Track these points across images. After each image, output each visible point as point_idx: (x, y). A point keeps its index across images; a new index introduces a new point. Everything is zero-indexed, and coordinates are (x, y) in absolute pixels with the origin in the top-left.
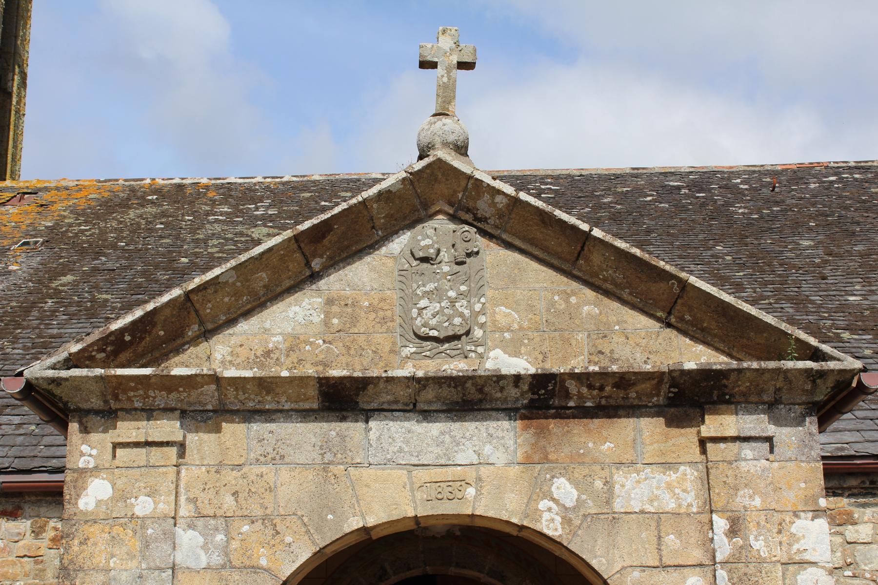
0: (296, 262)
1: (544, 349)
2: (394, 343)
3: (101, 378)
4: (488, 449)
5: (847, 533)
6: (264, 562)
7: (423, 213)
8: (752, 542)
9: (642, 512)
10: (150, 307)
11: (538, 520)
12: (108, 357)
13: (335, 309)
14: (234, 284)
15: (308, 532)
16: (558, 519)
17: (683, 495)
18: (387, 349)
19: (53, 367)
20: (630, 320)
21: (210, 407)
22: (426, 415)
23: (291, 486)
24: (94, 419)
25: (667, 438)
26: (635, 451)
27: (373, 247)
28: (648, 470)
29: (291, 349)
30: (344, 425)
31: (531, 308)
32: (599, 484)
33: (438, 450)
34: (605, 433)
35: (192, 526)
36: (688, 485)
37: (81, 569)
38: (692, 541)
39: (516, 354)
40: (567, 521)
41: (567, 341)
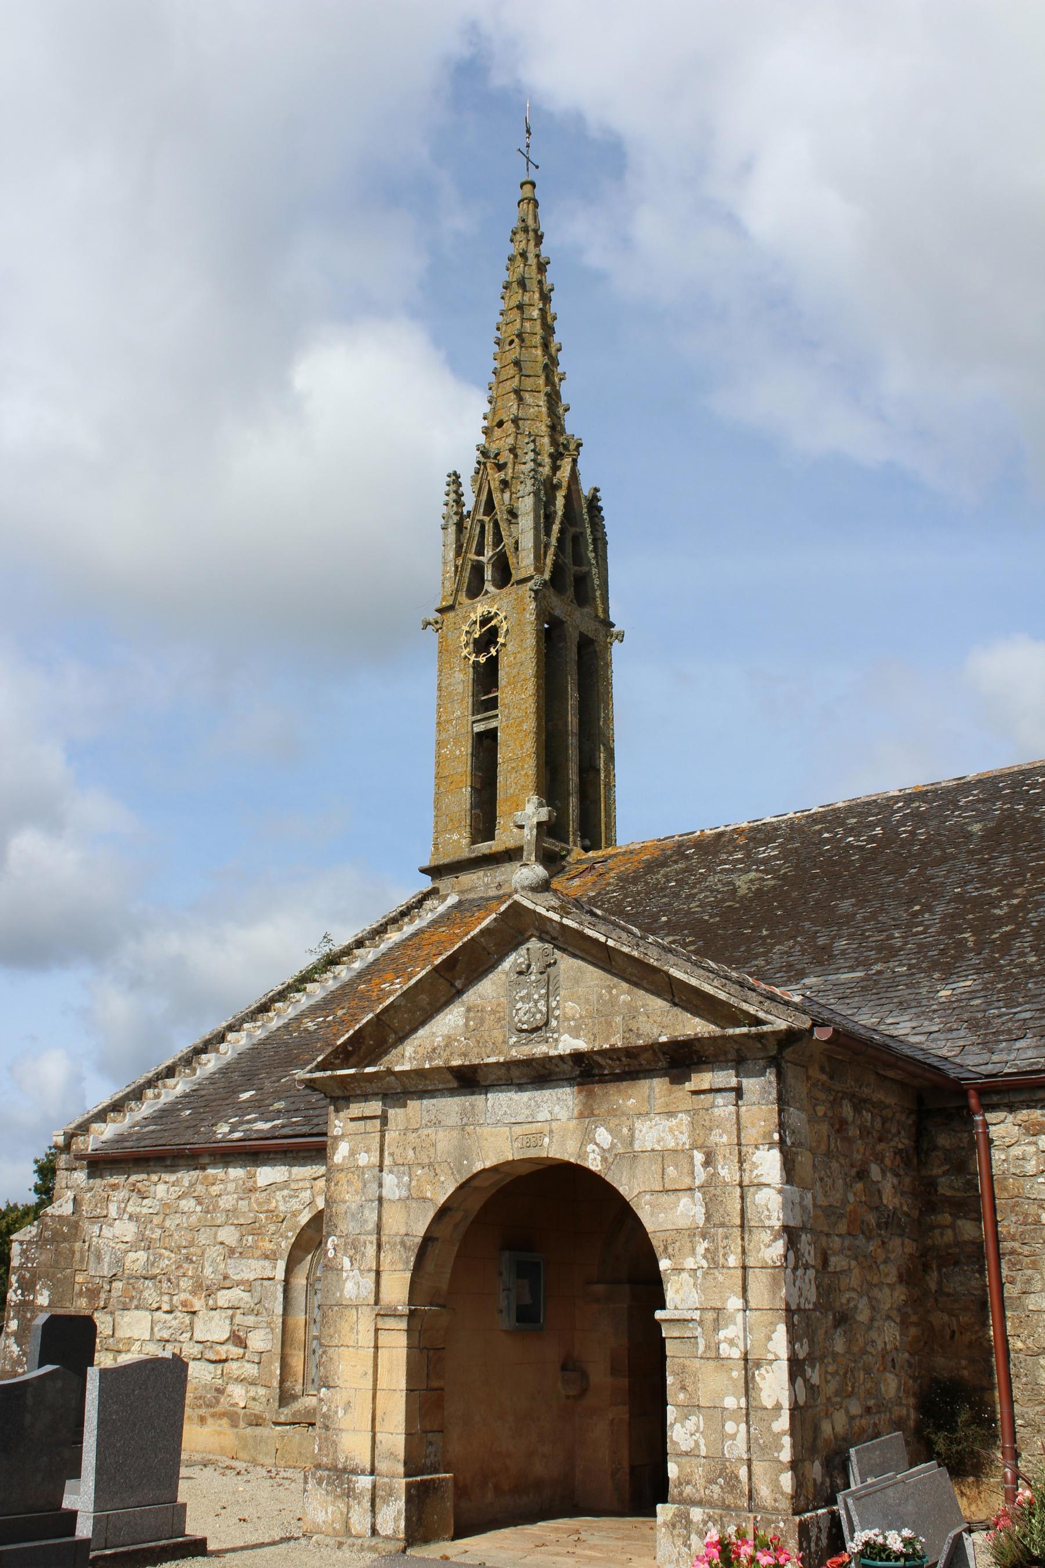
0: (443, 985)
1: (595, 1031)
2: (505, 1036)
3: (331, 1077)
4: (557, 1109)
5: (1040, 1142)
6: (429, 1195)
7: (520, 938)
8: (720, 1170)
9: (653, 1150)
10: (357, 1028)
11: (586, 1160)
12: (342, 1062)
13: (472, 1014)
14: (405, 1005)
15: (453, 1173)
16: (599, 1158)
17: (680, 1136)
18: (501, 1040)
19: (310, 1071)
20: (650, 1003)
21: (399, 1091)
22: (521, 1087)
23: (444, 1141)
24: (341, 1102)
25: (671, 1092)
26: (650, 1104)
27: (493, 967)
28: (657, 1118)
29: (447, 1046)
30: (474, 1097)
31: (587, 1001)
32: (625, 1130)
33: (528, 1112)
34: (630, 1092)
35: (391, 1172)
36: (684, 1128)
37: (335, 1202)
38: (685, 1171)
39: (577, 1037)
40: (604, 1159)
41: (609, 1024)
